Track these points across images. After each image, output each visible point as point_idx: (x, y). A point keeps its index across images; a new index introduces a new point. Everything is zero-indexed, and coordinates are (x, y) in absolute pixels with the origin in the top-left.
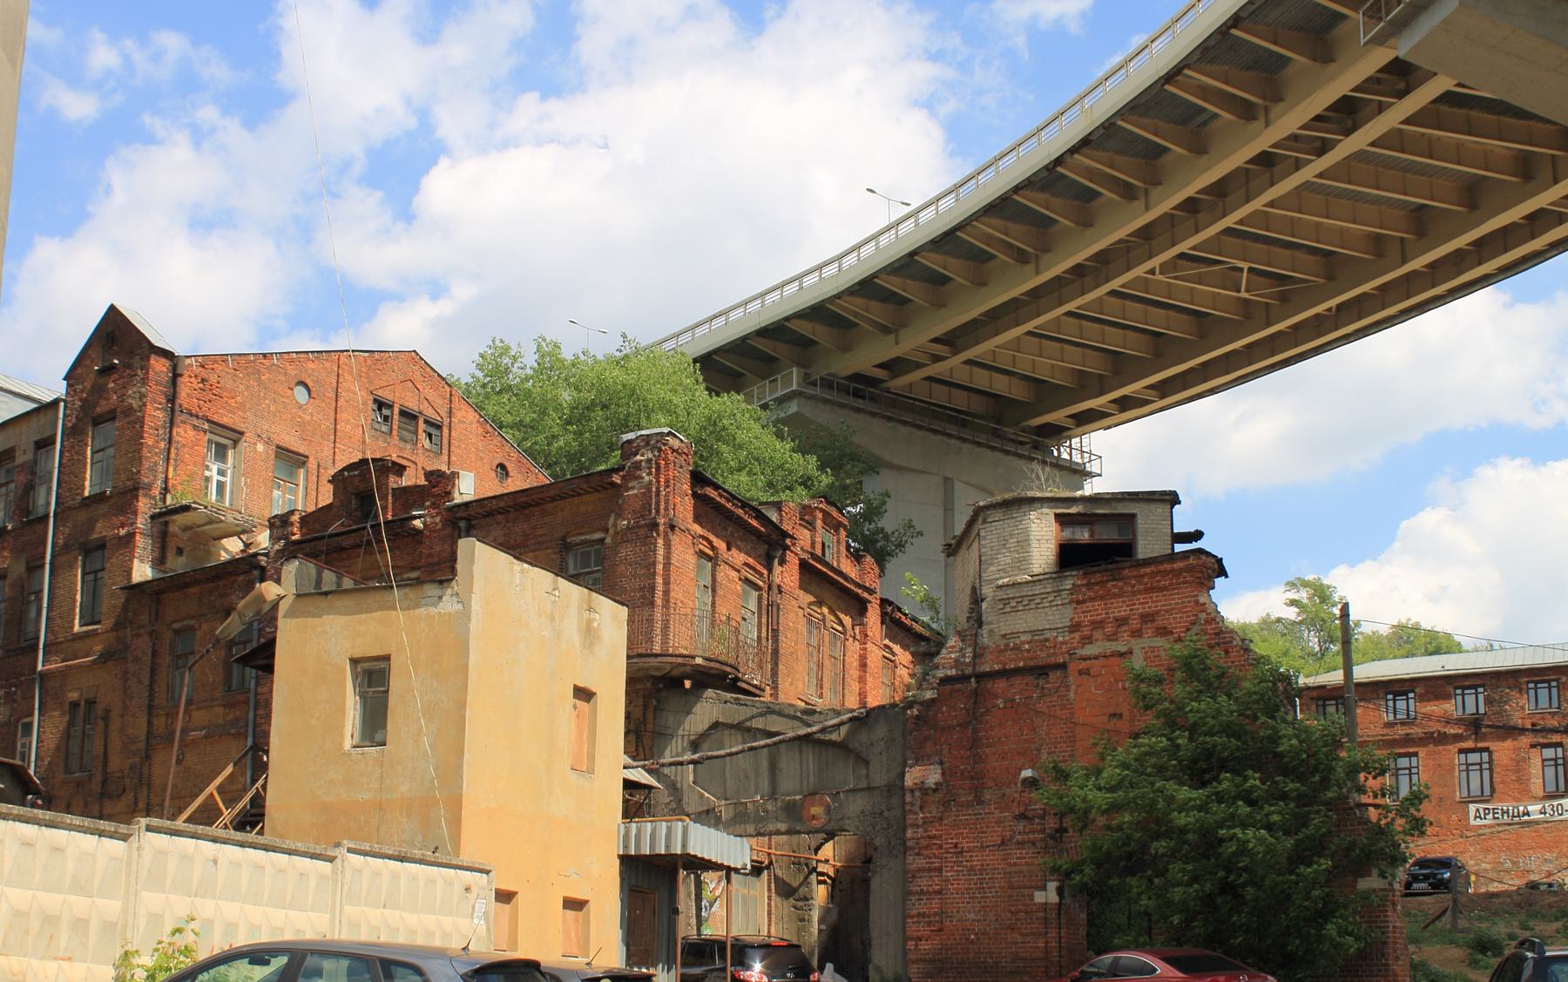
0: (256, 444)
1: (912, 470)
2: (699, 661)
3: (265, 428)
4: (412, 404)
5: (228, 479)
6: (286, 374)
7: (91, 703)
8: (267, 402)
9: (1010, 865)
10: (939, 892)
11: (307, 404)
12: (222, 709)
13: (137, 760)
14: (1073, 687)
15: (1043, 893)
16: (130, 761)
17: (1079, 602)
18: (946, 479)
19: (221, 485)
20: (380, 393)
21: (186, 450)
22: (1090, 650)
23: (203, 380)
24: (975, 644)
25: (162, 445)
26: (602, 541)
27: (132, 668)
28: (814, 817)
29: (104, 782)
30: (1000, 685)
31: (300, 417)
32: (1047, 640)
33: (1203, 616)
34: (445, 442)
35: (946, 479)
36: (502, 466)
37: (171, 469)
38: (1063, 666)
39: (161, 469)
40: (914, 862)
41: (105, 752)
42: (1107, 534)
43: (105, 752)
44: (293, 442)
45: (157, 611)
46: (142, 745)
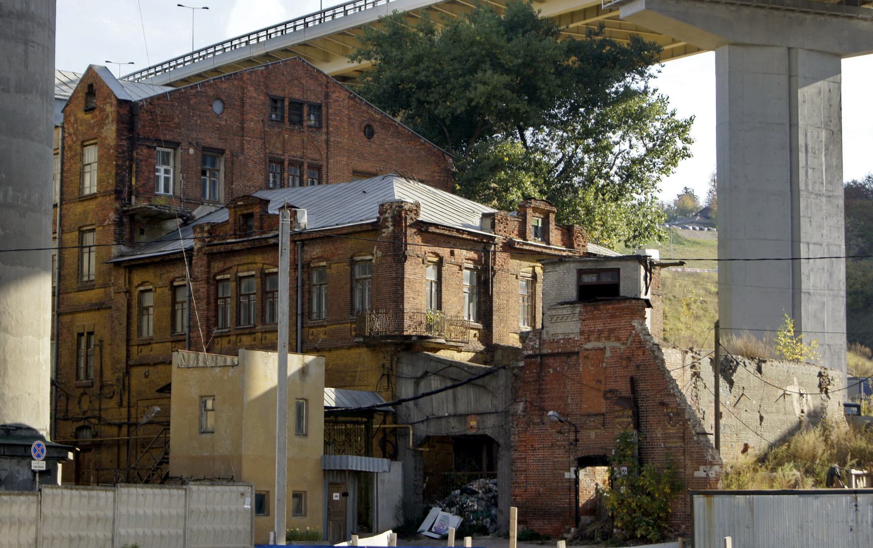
0: (188, 149)
1: (759, 45)
3: (194, 136)
4: (297, 95)
5: (171, 176)
8: (195, 118)
9: (555, 457)
10: (525, 471)
11: (222, 113)
12: (170, 344)
13: (121, 374)
14: (581, 365)
15: (568, 473)
16: (116, 375)
17: (583, 321)
18: (789, 49)
19: (167, 180)
22: (589, 346)
24: (540, 338)
26: (371, 260)
27: (115, 314)
28: (472, 427)
29: (101, 388)
30: (551, 361)
31: (217, 124)
32: (570, 339)
33: (634, 332)
34: (324, 117)
35: (789, 49)
36: (369, 126)
37: (134, 180)
38: (577, 353)
39: (127, 179)
40: (515, 455)
41: (101, 368)
42: (606, 279)
43: (101, 368)
44: (212, 140)
45: (129, 278)
46: (124, 365)
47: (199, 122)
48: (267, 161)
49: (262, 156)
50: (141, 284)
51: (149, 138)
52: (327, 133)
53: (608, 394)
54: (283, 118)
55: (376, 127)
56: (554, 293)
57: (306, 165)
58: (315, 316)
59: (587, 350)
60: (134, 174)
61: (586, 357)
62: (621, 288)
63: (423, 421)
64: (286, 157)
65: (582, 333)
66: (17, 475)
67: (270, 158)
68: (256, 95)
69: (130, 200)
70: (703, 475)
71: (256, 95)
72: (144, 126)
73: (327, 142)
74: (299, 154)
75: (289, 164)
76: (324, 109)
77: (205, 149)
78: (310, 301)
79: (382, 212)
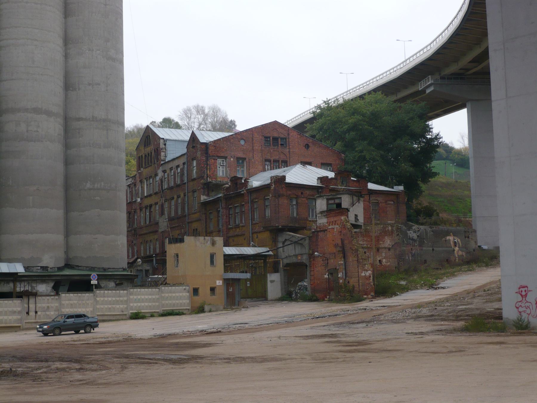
2: (280, 227)
4: (276, 135)
6: (237, 138)
7: (196, 229)
20: (266, 135)
21: (212, 165)
22: (330, 227)
23: (215, 146)
25: (206, 166)
26: (269, 198)
28: (299, 260)
36: (307, 145)
37: (208, 171)
38: (326, 230)
39: (206, 172)
44: (241, 155)
47: (234, 148)
48: (264, 161)
49: (262, 159)
50: (209, 211)
51: (214, 156)
52: (289, 148)
53: (336, 246)
54: (270, 144)
55: (310, 145)
56: (319, 208)
57: (280, 161)
58: (256, 220)
59: (329, 229)
60: (208, 170)
61: (329, 231)
62: (342, 204)
63: (285, 258)
64: (272, 159)
65: (327, 223)
66: (109, 285)
67: (265, 159)
68: (258, 137)
69: (207, 179)
70: (364, 275)
71: (258, 137)
72: (212, 152)
73: (289, 151)
74: (277, 157)
75: (273, 161)
76: (287, 140)
77: (237, 158)
78: (254, 215)
79: (271, 180)
